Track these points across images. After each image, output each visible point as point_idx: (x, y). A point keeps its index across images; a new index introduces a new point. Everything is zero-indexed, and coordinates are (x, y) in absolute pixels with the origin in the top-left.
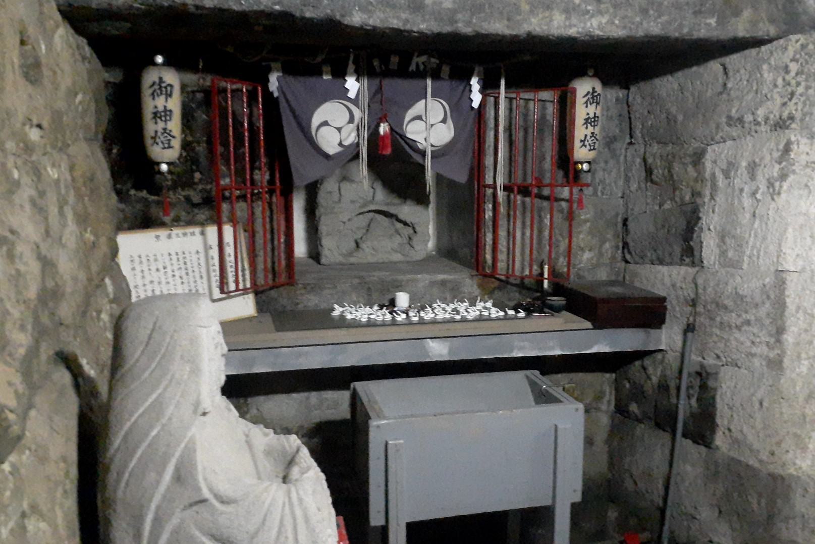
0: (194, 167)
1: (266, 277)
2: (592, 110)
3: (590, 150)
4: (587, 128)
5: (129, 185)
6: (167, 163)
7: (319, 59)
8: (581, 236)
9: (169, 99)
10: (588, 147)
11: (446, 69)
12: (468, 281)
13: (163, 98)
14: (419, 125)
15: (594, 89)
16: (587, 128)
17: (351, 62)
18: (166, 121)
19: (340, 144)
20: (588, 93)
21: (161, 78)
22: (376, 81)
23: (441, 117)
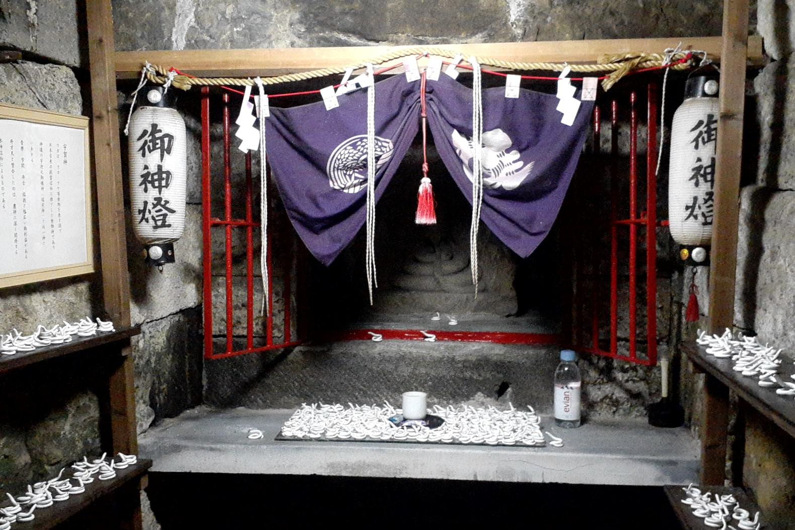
4: (697, 184)
10: (151, 222)
16: (146, 190)
18: (160, 188)
21: (154, 126)
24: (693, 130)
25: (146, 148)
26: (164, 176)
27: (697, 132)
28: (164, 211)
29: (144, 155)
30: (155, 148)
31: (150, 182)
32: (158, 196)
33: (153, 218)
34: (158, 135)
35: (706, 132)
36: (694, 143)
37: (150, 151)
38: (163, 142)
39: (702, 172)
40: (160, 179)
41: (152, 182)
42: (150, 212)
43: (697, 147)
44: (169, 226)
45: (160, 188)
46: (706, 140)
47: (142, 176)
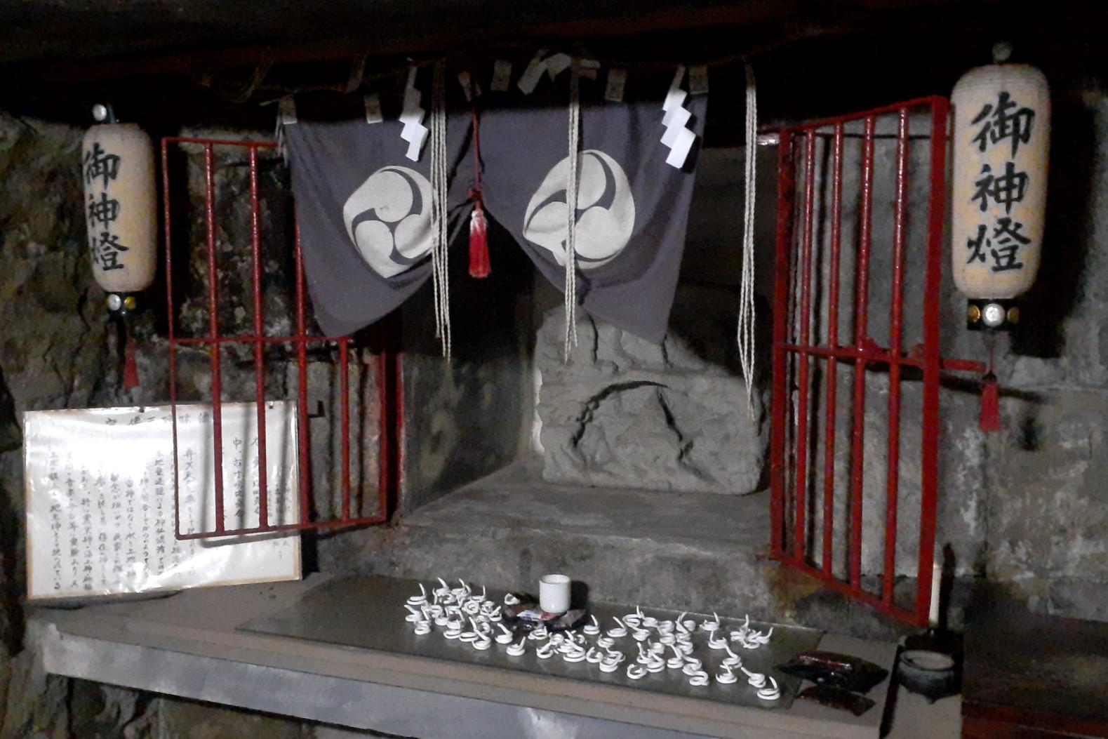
0: (235, 298)
1: (346, 504)
2: (999, 155)
3: (998, 269)
4: (984, 207)
5: (149, 327)
6: (119, 294)
7: (353, 85)
8: (1059, 495)
9: (110, 181)
10: (991, 261)
11: (617, 80)
12: (746, 569)
13: (100, 179)
14: (559, 213)
15: (1004, 97)
16: (984, 207)
17: (410, 86)
18: (106, 220)
19: (396, 256)
20: (987, 109)
21: (96, 146)
22: (467, 120)
23: (599, 193)
24: (977, 120)
25: (988, 135)
26: (110, 206)
27: (982, 124)
28: (113, 249)
29: (983, 148)
30: (1003, 135)
31: (991, 193)
32: (104, 230)
33: (994, 253)
34: (101, 157)
35: (996, 123)
36: (979, 142)
37: (995, 141)
38: (106, 165)
39: (992, 187)
40: (106, 210)
41: (996, 194)
42: (989, 243)
43: (983, 148)
44: (121, 266)
45: (106, 220)
46: (997, 135)
47: (978, 184)
